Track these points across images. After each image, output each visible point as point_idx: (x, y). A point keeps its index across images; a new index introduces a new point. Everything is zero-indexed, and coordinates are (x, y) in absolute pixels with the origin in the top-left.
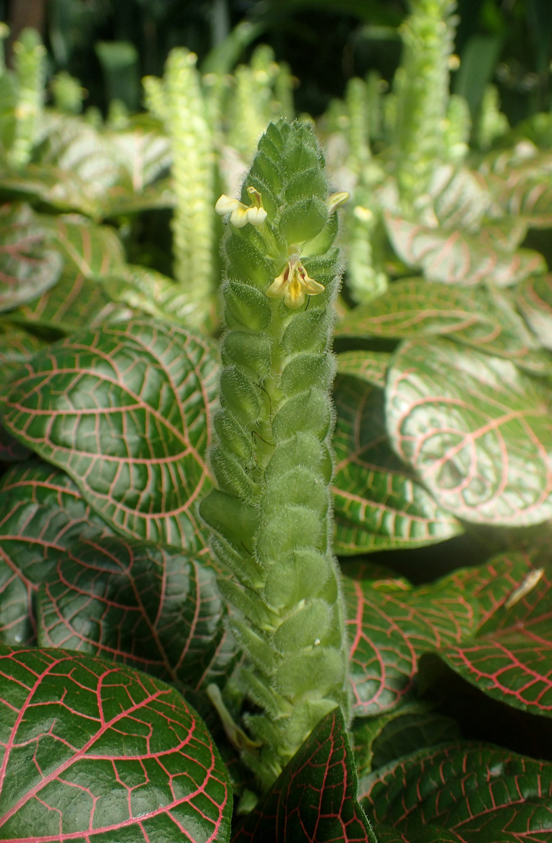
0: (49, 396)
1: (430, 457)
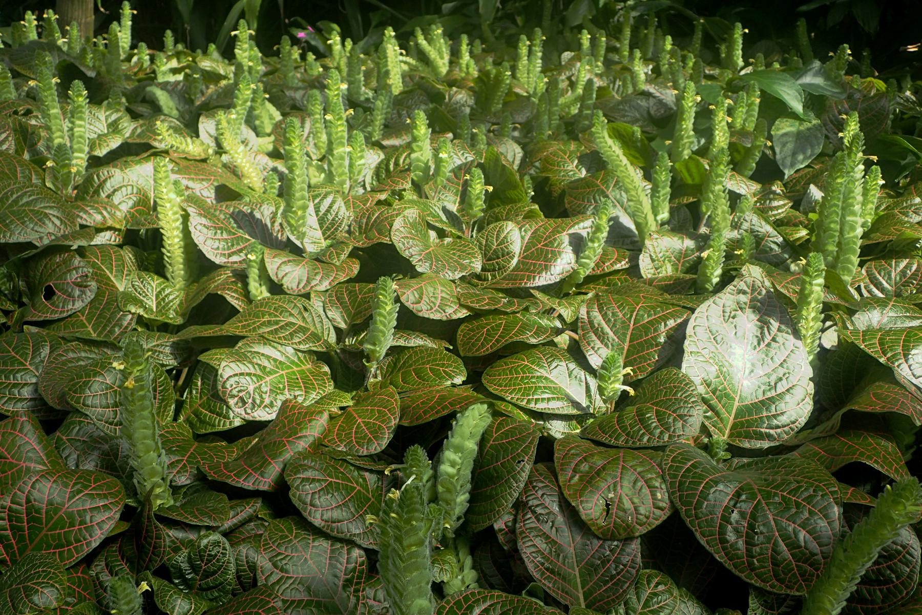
0: (82, 391)
1: (233, 396)
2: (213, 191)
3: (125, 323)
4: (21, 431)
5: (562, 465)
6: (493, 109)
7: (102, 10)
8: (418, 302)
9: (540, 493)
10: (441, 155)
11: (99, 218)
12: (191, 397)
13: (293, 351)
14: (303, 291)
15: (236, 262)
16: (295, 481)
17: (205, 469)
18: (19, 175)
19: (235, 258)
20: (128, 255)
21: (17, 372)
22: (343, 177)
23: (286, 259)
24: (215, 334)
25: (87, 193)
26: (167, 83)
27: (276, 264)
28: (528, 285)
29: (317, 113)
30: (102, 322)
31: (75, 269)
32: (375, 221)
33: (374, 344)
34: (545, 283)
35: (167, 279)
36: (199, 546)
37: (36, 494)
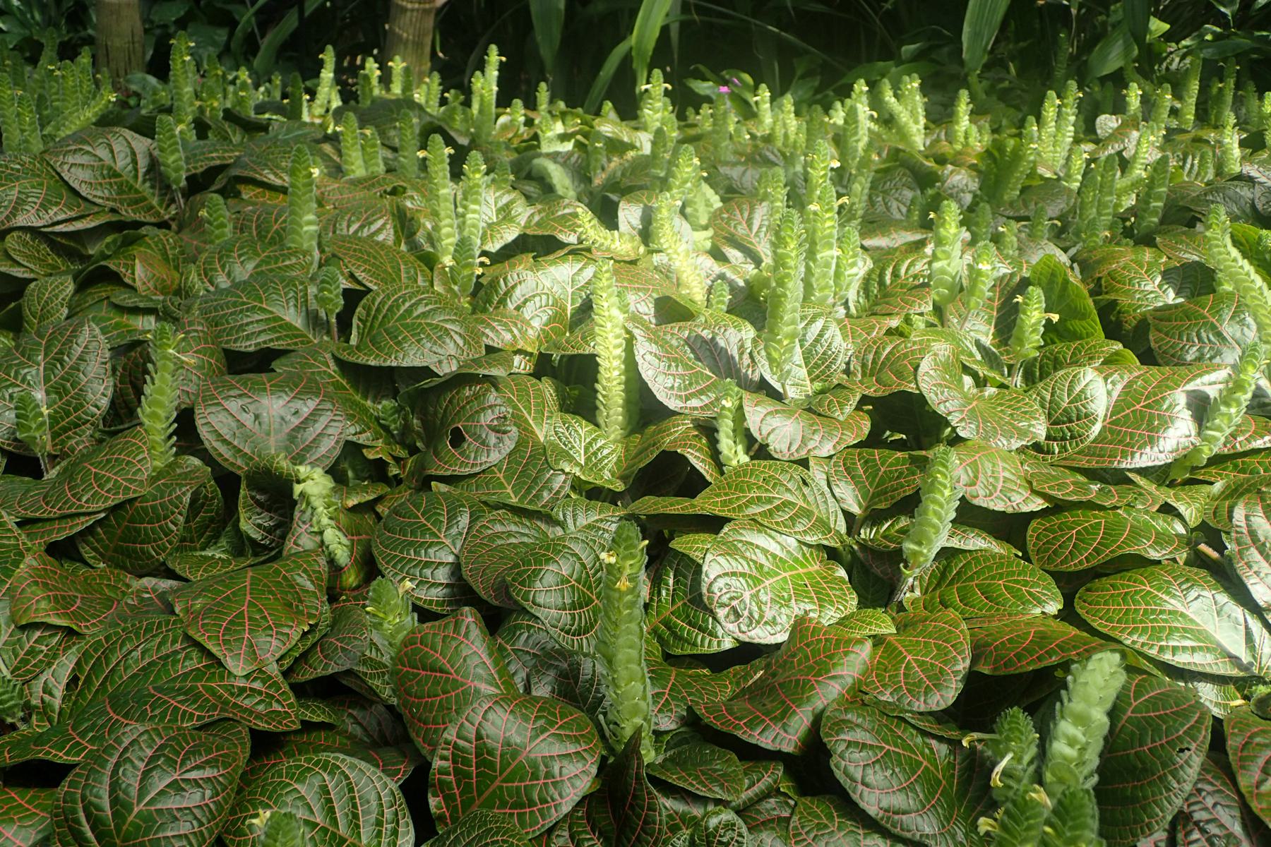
1: (723, 605)
2: (651, 305)
3: (556, 486)
4: (466, 635)
5: (1241, 759)
6: (1006, 197)
7: (441, 55)
8: (973, 484)
9: (1210, 801)
10: (980, 266)
11: (508, 336)
12: (660, 601)
13: (795, 544)
14: (796, 457)
15: (695, 409)
16: (837, 743)
17: (700, 711)
18: (403, 275)
19: (695, 403)
20: (547, 388)
21: (429, 547)
22: (827, 292)
23: (771, 408)
24: (686, 512)
25: (490, 302)
26: (557, 153)
27: (758, 416)
28: (1123, 466)
29: (778, 199)
30: (525, 483)
31: (490, 407)
32: (887, 357)
33: (920, 544)
34: (1150, 464)
35: (597, 425)
36: (707, 828)
37: (488, 729)
